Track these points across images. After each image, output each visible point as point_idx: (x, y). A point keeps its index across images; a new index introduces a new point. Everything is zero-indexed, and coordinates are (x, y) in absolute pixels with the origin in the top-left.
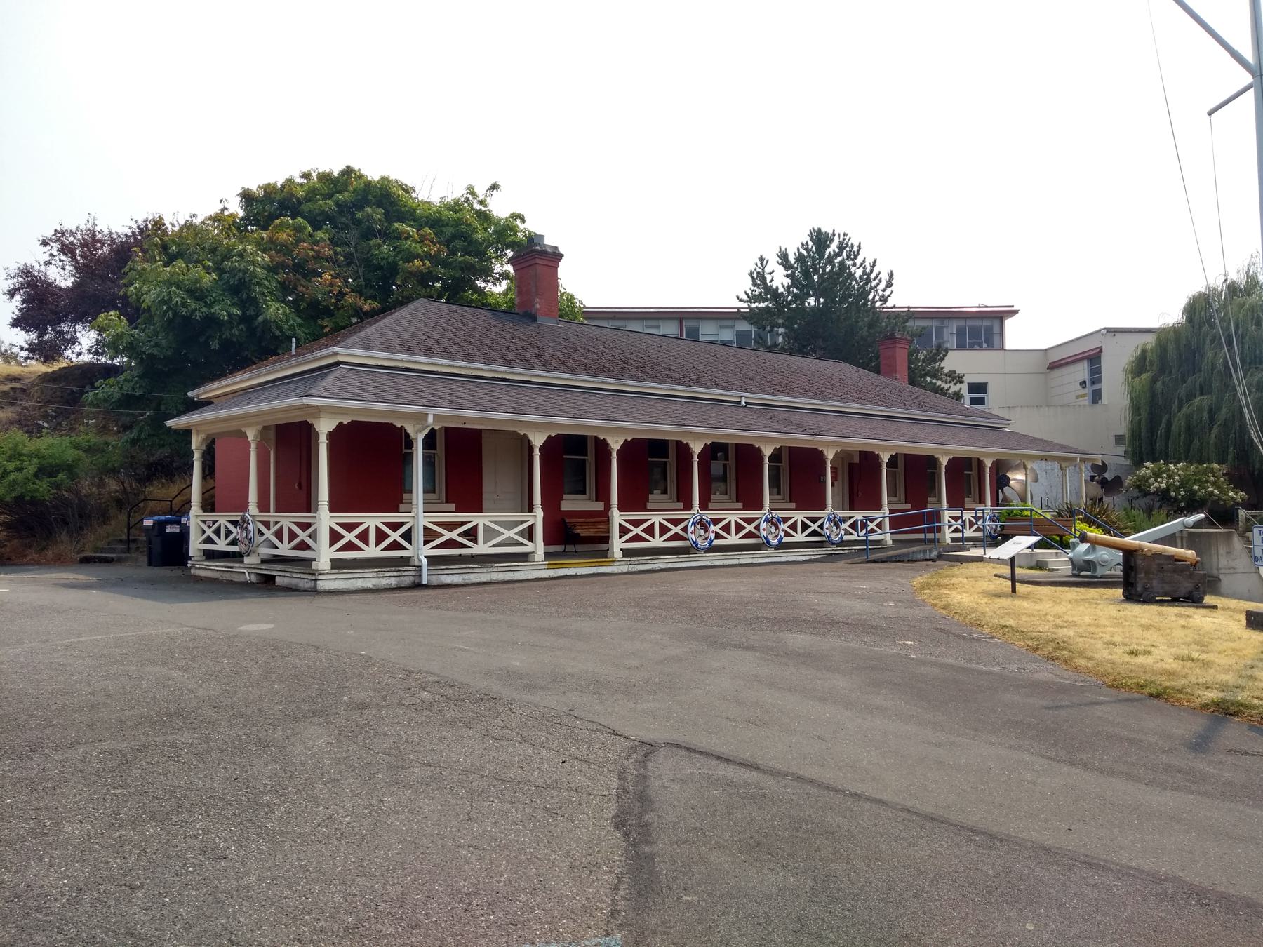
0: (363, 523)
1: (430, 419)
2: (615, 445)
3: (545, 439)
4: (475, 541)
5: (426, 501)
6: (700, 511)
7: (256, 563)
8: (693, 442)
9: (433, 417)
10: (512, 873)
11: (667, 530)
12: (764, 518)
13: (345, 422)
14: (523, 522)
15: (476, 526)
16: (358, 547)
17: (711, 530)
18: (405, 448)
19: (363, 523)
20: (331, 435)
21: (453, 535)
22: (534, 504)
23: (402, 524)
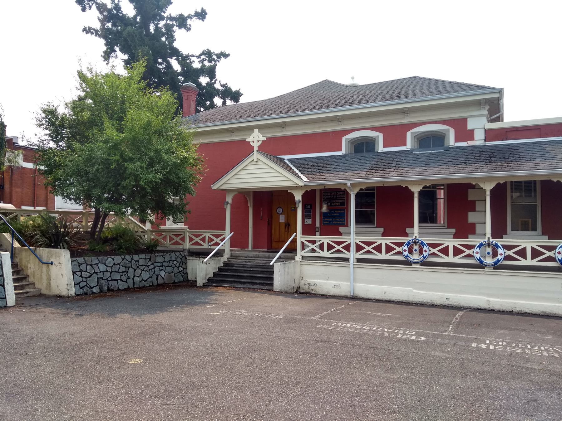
6: (491, 238)
11: (539, 254)
15: (381, 244)
20: (492, 191)
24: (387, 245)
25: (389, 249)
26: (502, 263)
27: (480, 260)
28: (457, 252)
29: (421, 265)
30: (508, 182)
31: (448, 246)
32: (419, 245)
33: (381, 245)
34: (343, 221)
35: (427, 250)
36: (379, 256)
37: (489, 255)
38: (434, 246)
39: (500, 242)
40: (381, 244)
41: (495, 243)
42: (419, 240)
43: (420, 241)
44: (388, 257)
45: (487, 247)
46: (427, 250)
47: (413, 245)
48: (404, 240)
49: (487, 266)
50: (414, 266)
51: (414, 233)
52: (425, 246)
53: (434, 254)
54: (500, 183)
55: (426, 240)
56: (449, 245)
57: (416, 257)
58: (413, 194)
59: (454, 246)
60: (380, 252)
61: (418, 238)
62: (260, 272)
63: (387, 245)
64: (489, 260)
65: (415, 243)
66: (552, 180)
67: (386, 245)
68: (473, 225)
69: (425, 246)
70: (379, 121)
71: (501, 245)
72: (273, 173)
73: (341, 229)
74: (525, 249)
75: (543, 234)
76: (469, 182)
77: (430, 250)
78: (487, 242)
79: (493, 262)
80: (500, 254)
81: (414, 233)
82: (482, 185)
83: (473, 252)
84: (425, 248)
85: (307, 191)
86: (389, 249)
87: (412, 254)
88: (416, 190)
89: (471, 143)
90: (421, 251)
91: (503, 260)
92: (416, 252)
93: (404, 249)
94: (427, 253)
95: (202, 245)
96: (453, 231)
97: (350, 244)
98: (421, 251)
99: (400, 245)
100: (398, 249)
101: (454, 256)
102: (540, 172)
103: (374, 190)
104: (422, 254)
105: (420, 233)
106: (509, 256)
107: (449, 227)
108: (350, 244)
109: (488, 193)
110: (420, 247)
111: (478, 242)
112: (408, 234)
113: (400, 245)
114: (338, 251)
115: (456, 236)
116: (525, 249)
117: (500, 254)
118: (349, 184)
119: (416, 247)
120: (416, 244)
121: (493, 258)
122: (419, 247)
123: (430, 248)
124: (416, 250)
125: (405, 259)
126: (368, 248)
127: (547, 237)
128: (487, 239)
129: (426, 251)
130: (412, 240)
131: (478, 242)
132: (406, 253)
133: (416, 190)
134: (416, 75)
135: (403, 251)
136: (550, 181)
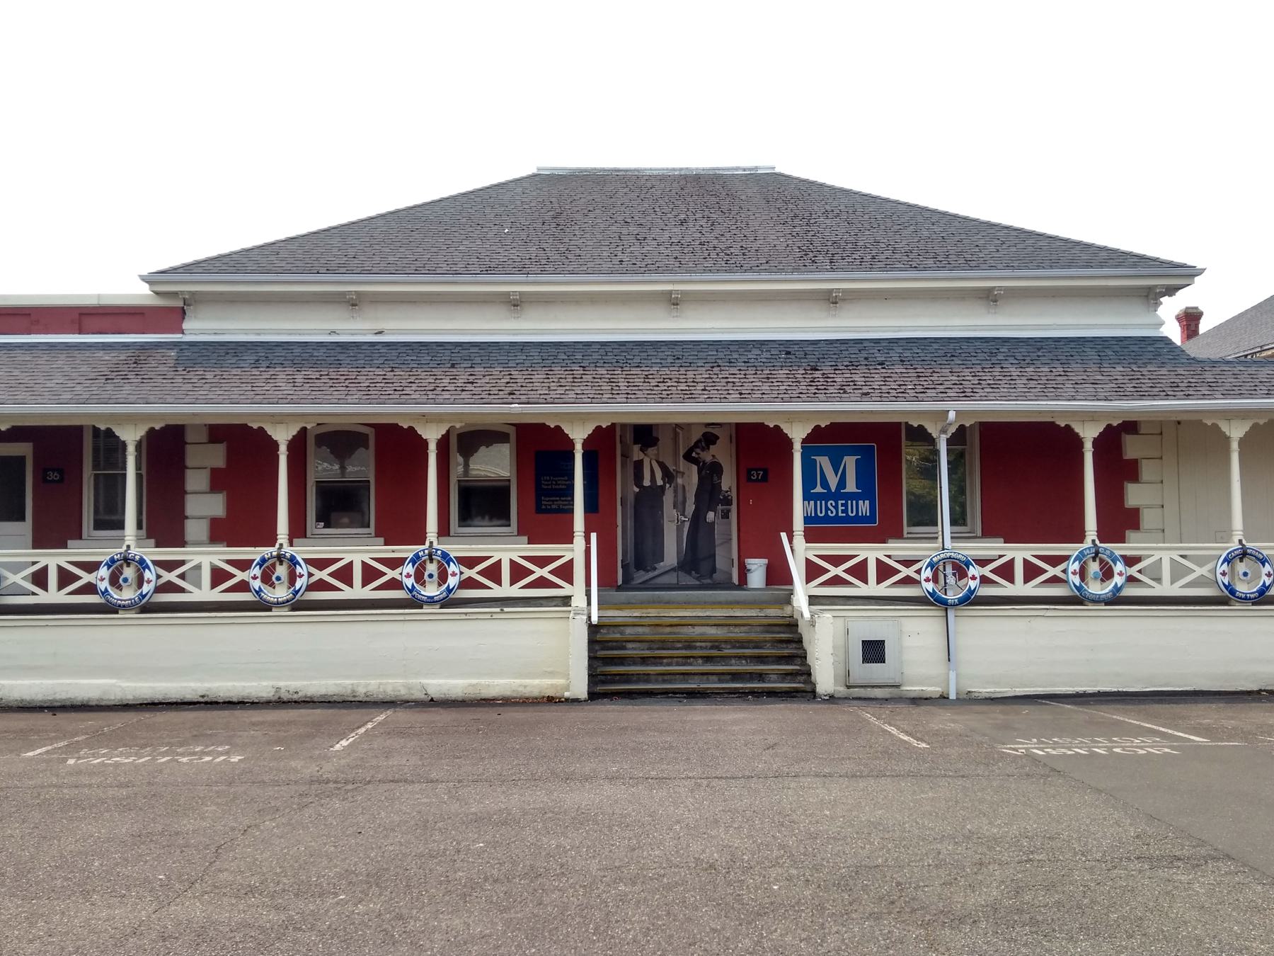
0: (38, 562)
1: (952, 415)
2: (131, 436)
3: (590, 433)
4: (350, 583)
5: (139, 538)
6: (1097, 542)
7: (1076, 583)
8: (789, 425)
9: (955, 410)
10: (742, 850)
11: (1038, 571)
12: (928, 560)
13: (1115, 424)
14: (34, 563)
15: (866, 560)
16: (1136, 578)
17: (970, 575)
18: (21, 460)
19: (38, 562)
20: (1096, 442)
21: (544, 572)
22: (1086, 529)
23: (182, 563)
25: (1031, 572)
26: (303, 598)
27: (1079, 588)
29: (293, 609)
30: (88, 426)
31: (866, 559)
32: (439, 562)
33: (1011, 562)
34: (569, 501)
35: (457, 571)
37: (431, 580)
39: (1118, 549)
40: (866, 560)
41: (292, 555)
42: (437, 550)
44: (1031, 589)
46: (457, 571)
48: (407, 551)
49: (124, 606)
50: (426, 610)
54: (600, 426)
55: (456, 549)
56: (47, 566)
57: (281, 593)
59: (1025, 560)
60: (1011, 579)
61: (435, 545)
62: (680, 660)
64: (281, 593)
67: (1026, 562)
68: (1135, 512)
71: (454, 557)
74: (350, 566)
75: (520, 533)
76: (396, 422)
77: (461, 573)
79: (1255, 590)
80: (1118, 574)
81: (126, 538)
82: (1224, 427)
83: (401, 574)
84: (453, 568)
85: (598, 428)
86: (1031, 572)
87: (423, 584)
90: (443, 577)
91: (306, 590)
94: (152, 586)
97: (571, 561)
98: (292, 578)
99: (244, 565)
100: (390, 574)
102: (152, 409)
104: (445, 583)
108: (571, 561)
109: (131, 450)
110: (440, 566)
111: (411, 551)
114: (542, 583)
116: (350, 566)
117: (1118, 574)
120: (128, 565)
121: (440, 585)
122: (439, 568)
123: (464, 569)
124: (431, 576)
125: (254, 599)
126: (834, 571)
127: (225, 544)
128: (124, 548)
129: (454, 574)
131: (411, 551)
132: (256, 584)
135: (251, 579)
136: (244, 427)
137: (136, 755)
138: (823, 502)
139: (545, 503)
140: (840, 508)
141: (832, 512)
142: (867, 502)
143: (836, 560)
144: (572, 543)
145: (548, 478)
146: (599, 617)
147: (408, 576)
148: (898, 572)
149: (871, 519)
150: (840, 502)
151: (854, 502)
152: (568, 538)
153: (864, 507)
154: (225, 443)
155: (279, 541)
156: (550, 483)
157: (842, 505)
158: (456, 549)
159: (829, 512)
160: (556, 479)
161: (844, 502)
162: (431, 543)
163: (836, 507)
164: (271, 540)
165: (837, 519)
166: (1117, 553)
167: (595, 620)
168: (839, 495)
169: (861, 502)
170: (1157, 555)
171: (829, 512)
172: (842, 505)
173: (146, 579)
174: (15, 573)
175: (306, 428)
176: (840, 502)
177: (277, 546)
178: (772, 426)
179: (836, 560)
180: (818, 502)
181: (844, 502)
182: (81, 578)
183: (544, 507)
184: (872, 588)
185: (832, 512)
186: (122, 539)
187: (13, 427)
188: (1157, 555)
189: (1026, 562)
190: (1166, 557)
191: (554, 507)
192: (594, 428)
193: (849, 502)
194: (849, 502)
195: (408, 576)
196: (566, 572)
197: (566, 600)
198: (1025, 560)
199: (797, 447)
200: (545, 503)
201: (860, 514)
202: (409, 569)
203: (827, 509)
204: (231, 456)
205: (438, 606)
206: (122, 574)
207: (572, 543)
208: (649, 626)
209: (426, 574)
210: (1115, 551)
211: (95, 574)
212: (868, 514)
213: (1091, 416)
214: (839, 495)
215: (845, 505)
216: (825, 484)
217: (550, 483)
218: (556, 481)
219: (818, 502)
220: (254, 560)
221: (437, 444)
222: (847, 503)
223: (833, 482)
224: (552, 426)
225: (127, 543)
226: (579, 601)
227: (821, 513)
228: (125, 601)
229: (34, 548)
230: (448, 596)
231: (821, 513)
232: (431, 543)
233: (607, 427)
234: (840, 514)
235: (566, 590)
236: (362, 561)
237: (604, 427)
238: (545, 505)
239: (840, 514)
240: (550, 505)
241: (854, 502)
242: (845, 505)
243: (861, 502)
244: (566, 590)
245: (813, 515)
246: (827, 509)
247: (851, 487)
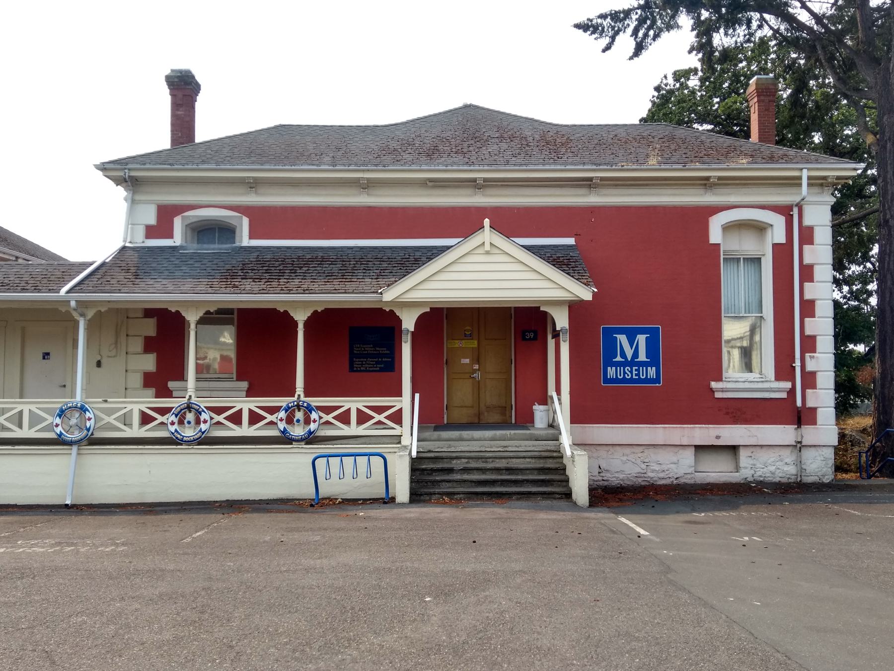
6: (302, 396)
20: (307, 324)
24: (359, 411)
25: (255, 418)
28: (255, 418)
33: (240, 411)
36: (345, 431)
38: (219, 411)
42: (304, 402)
43: (305, 404)
45: (297, 410)
46: (208, 418)
47: (294, 411)
48: (282, 401)
51: (194, 390)
52: (87, 412)
53: (328, 423)
58: (295, 324)
59: (250, 409)
61: (302, 398)
63: (359, 411)
64: (298, 431)
65: (299, 407)
66: (60, 309)
67: (251, 411)
69: (87, 412)
70: (550, 196)
71: (205, 407)
72: (520, 273)
73: (171, 385)
78: (296, 403)
83: (277, 418)
85: (315, 312)
88: (301, 317)
89: (234, 245)
92: (189, 426)
93: (279, 418)
95: (12, 431)
96: (245, 385)
97: (400, 410)
100: (270, 418)
101: (357, 424)
103: (233, 314)
105: (197, 389)
106: (219, 423)
107: (240, 378)
108: (400, 410)
110: (305, 414)
112: (172, 391)
113: (163, 411)
115: (250, 393)
118: (73, 304)
119: (299, 415)
123: (213, 415)
126: (378, 417)
128: (295, 398)
130: (293, 402)
133: (301, 317)
134: (277, 123)
135: (278, 421)
136: (274, 310)
137: (14, 553)
138: (622, 368)
139: (356, 366)
140: (634, 372)
141: (628, 376)
142: (654, 368)
143: (379, 410)
144: (402, 397)
145: (359, 346)
146: (417, 452)
147: (281, 420)
148: (226, 418)
149: (657, 380)
150: (634, 368)
151: (644, 368)
152: (397, 392)
153: (652, 372)
154: (156, 318)
155: (297, 393)
156: (360, 349)
157: (636, 370)
158: (315, 401)
159: (626, 375)
160: (365, 346)
161: (637, 368)
162: (299, 396)
163: (631, 372)
164: (291, 392)
165: (632, 380)
166: (313, 404)
167: (414, 454)
168: (633, 363)
169: (649, 368)
170: (129, 407)
171: (626, 375)
172: (636, 370)
173: (312, 419)
174: (328, 414)
175: (100, 311)
176: (634, 368)
177: (296, 396)
178: (388, 310)
179: (379, 410)
180: (618, 368)
181: (637, 368)
182: (224, 418)
183: (355, 369)
184: (353, 429)
185: (628, 376)
186: (186, 390)
187: (326, 309)
188: (19, 408)
189: (251, 411)
190: (26, 409)
191: (362, 369)
192: (312, 312)
193: (641, 368)
194: (641, 368)
195: (281, 420)
196: (397, 418)
197: (398, 439)
198: (250, 409)
199: (193, 326)
200: (356, 366)
201: (649, 377)
202: (282, 414)
203: (625, 373)
204: (160, 327)
205: (303, 443)
206: (185, 418)
207: (402, 397)
208: (531, 458)
209: (295, 420)
210: (311, 403)
211: (276, 415)
212: (655, 377)
213: (305, 304)
214: (633, 363)
215: (638, 370)
216: (623, 355)
217: (360, 349)
218: (364, 348)
219: (618, 368)
220: (282, 407)
221: (304, 324)
222: (639, 369)
223: (629, 353)
224: (388, 310)
225: (189, 394)
226: (405, 441)
227: (620, 376)
228: (189, 437)
229: (156, 397)
230: (309, 437)
231: (620, 376)
232: (299, 396)
233: (322, 311)
234: (634, 377)
235: (397, 431)
236: (249, 409)
237: (319, 311)
238: (357, 367)
239: (634, 377)
240: (360, 368)
241: (644, 368)
242: (638, 370)
243: (649, 368)
244: (397, 431)
245: (614, 377)
246: (625, 373)
247: (642, 357)
